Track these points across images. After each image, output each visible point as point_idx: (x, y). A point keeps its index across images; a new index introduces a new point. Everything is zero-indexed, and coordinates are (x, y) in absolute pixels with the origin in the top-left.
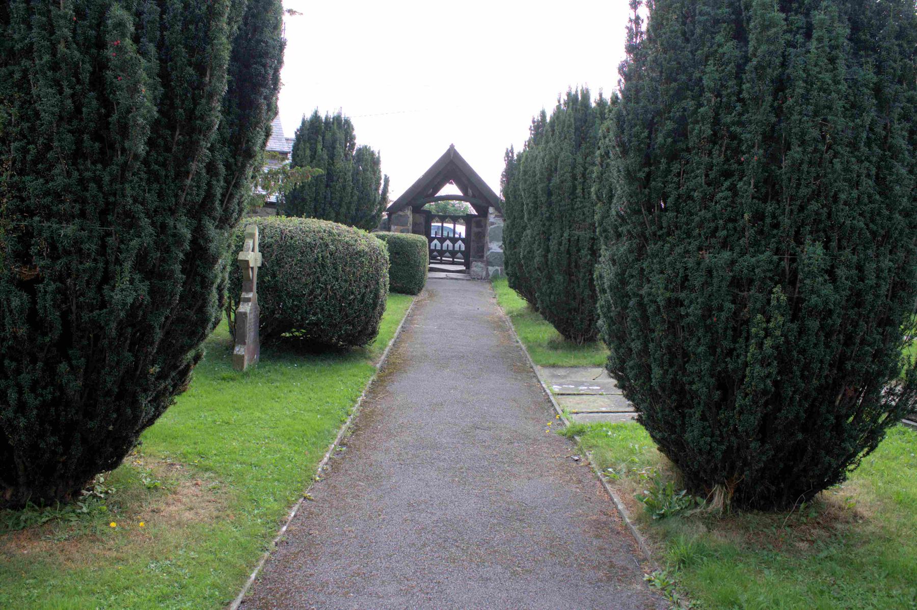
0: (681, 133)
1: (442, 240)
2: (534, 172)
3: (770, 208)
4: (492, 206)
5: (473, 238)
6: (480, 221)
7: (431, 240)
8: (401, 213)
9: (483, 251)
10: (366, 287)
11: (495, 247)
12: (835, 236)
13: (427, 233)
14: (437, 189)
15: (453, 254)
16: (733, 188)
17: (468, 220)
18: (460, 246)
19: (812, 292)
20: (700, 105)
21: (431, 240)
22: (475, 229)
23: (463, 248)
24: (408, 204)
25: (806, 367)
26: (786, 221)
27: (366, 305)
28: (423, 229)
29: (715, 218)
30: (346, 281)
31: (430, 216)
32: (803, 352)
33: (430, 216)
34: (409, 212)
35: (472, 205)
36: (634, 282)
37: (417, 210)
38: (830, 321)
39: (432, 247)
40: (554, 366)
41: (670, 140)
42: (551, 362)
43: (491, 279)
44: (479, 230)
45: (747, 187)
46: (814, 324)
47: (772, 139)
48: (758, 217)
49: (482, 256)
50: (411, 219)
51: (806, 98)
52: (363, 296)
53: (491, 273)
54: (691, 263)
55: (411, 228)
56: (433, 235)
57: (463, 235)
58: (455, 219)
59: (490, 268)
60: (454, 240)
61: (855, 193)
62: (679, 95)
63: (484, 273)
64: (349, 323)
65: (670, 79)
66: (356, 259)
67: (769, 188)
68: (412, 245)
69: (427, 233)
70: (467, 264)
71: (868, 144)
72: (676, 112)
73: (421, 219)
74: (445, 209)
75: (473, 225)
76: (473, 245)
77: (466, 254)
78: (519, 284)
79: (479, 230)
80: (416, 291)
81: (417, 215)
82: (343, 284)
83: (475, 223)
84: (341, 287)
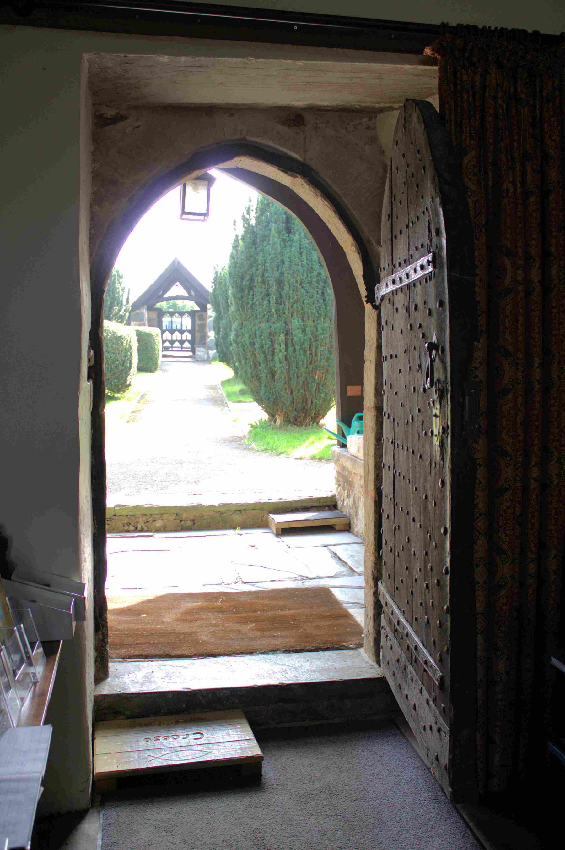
0: (252, 280)
1: (172, 332)
2: (225, 283)
3: (281, 307)
4: (209, 303)
5: (197, 328)
6: (202, 315)
7: (163, 332)
8: (138, 311)
9: (205, 340)
10: (125, 356)
11: (212, 335)
12: (306, 316)
13: (160, 326)
14: (165, 291)
15: (182, 342)
16: (269, 301)
17: (192, 314)
18: (187, 336)
19: (295, 336)
20: (257, 270)
21: (163, 332)
22: (198, 322)
23: (189, 338)
24: (143, 305)
25: (297, 363)
26: (287, 311)
27: (125, 367)
28: (155, 322)
29: (263, 312)
30: (114, 353)
31: (161, 313)
32: (296, 358)
33: (161, 313)
34: (144, 311)
35: (196, 303)
36: (240, 337)
37: (150, 308)
38: (304, 346)
39: (164, 338)
40: (240, 402)
41: (248, 283)
42: (239, 400)
43: (208, 361)
44: (202, 322)
45: (273, 300)
46: (298, 348)
47: (280, 283)
48: (277, 311)
49: (204, 344)
50: (146, 315)
51: (290, 268)
52: (124, 362)
53: (211, 356)
54: (256, 328)
55: (146, 323)
56: (164, 328)
57: (189, 328)
58: (182, 314)
59: (210, 352)
60: (182, 332)
61: (311, 300)
62: (251, 266)
63: (206, 356)
64: (116, 378)
65: (248, 259)
66: (119, 340)
67: (280, 301)
68: (150, 335)
69: (160, 326)
70: (193, 350)
71: (318, 282)
72: (250, 272)
73: (154, 315)
74: (175, 306)
75: (197, 318)
76: (197, 335)
77: (192, 342)
78: (224, 357)
79: (202, 322)
80: (153, 369)
81: (151, 313)
82: (112, 355)
83: (197, 316)
84: (111, 357)
